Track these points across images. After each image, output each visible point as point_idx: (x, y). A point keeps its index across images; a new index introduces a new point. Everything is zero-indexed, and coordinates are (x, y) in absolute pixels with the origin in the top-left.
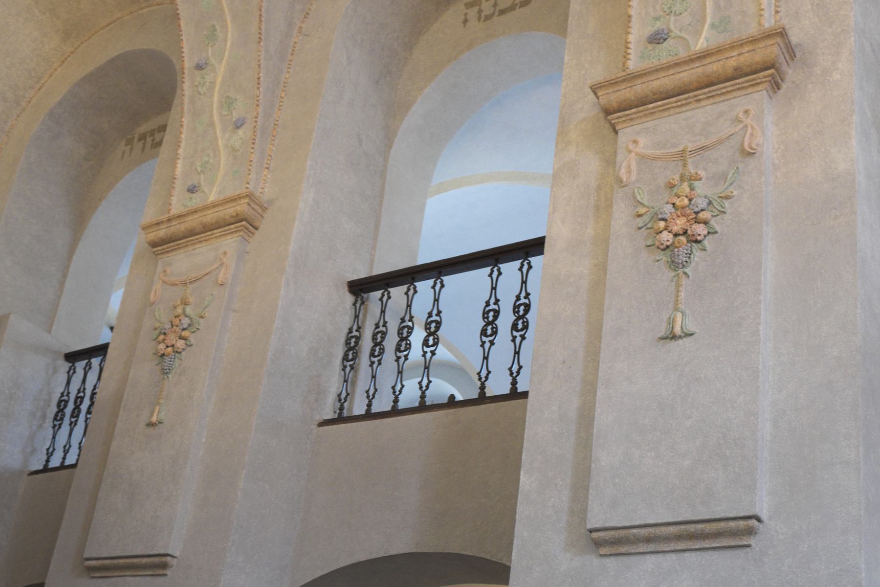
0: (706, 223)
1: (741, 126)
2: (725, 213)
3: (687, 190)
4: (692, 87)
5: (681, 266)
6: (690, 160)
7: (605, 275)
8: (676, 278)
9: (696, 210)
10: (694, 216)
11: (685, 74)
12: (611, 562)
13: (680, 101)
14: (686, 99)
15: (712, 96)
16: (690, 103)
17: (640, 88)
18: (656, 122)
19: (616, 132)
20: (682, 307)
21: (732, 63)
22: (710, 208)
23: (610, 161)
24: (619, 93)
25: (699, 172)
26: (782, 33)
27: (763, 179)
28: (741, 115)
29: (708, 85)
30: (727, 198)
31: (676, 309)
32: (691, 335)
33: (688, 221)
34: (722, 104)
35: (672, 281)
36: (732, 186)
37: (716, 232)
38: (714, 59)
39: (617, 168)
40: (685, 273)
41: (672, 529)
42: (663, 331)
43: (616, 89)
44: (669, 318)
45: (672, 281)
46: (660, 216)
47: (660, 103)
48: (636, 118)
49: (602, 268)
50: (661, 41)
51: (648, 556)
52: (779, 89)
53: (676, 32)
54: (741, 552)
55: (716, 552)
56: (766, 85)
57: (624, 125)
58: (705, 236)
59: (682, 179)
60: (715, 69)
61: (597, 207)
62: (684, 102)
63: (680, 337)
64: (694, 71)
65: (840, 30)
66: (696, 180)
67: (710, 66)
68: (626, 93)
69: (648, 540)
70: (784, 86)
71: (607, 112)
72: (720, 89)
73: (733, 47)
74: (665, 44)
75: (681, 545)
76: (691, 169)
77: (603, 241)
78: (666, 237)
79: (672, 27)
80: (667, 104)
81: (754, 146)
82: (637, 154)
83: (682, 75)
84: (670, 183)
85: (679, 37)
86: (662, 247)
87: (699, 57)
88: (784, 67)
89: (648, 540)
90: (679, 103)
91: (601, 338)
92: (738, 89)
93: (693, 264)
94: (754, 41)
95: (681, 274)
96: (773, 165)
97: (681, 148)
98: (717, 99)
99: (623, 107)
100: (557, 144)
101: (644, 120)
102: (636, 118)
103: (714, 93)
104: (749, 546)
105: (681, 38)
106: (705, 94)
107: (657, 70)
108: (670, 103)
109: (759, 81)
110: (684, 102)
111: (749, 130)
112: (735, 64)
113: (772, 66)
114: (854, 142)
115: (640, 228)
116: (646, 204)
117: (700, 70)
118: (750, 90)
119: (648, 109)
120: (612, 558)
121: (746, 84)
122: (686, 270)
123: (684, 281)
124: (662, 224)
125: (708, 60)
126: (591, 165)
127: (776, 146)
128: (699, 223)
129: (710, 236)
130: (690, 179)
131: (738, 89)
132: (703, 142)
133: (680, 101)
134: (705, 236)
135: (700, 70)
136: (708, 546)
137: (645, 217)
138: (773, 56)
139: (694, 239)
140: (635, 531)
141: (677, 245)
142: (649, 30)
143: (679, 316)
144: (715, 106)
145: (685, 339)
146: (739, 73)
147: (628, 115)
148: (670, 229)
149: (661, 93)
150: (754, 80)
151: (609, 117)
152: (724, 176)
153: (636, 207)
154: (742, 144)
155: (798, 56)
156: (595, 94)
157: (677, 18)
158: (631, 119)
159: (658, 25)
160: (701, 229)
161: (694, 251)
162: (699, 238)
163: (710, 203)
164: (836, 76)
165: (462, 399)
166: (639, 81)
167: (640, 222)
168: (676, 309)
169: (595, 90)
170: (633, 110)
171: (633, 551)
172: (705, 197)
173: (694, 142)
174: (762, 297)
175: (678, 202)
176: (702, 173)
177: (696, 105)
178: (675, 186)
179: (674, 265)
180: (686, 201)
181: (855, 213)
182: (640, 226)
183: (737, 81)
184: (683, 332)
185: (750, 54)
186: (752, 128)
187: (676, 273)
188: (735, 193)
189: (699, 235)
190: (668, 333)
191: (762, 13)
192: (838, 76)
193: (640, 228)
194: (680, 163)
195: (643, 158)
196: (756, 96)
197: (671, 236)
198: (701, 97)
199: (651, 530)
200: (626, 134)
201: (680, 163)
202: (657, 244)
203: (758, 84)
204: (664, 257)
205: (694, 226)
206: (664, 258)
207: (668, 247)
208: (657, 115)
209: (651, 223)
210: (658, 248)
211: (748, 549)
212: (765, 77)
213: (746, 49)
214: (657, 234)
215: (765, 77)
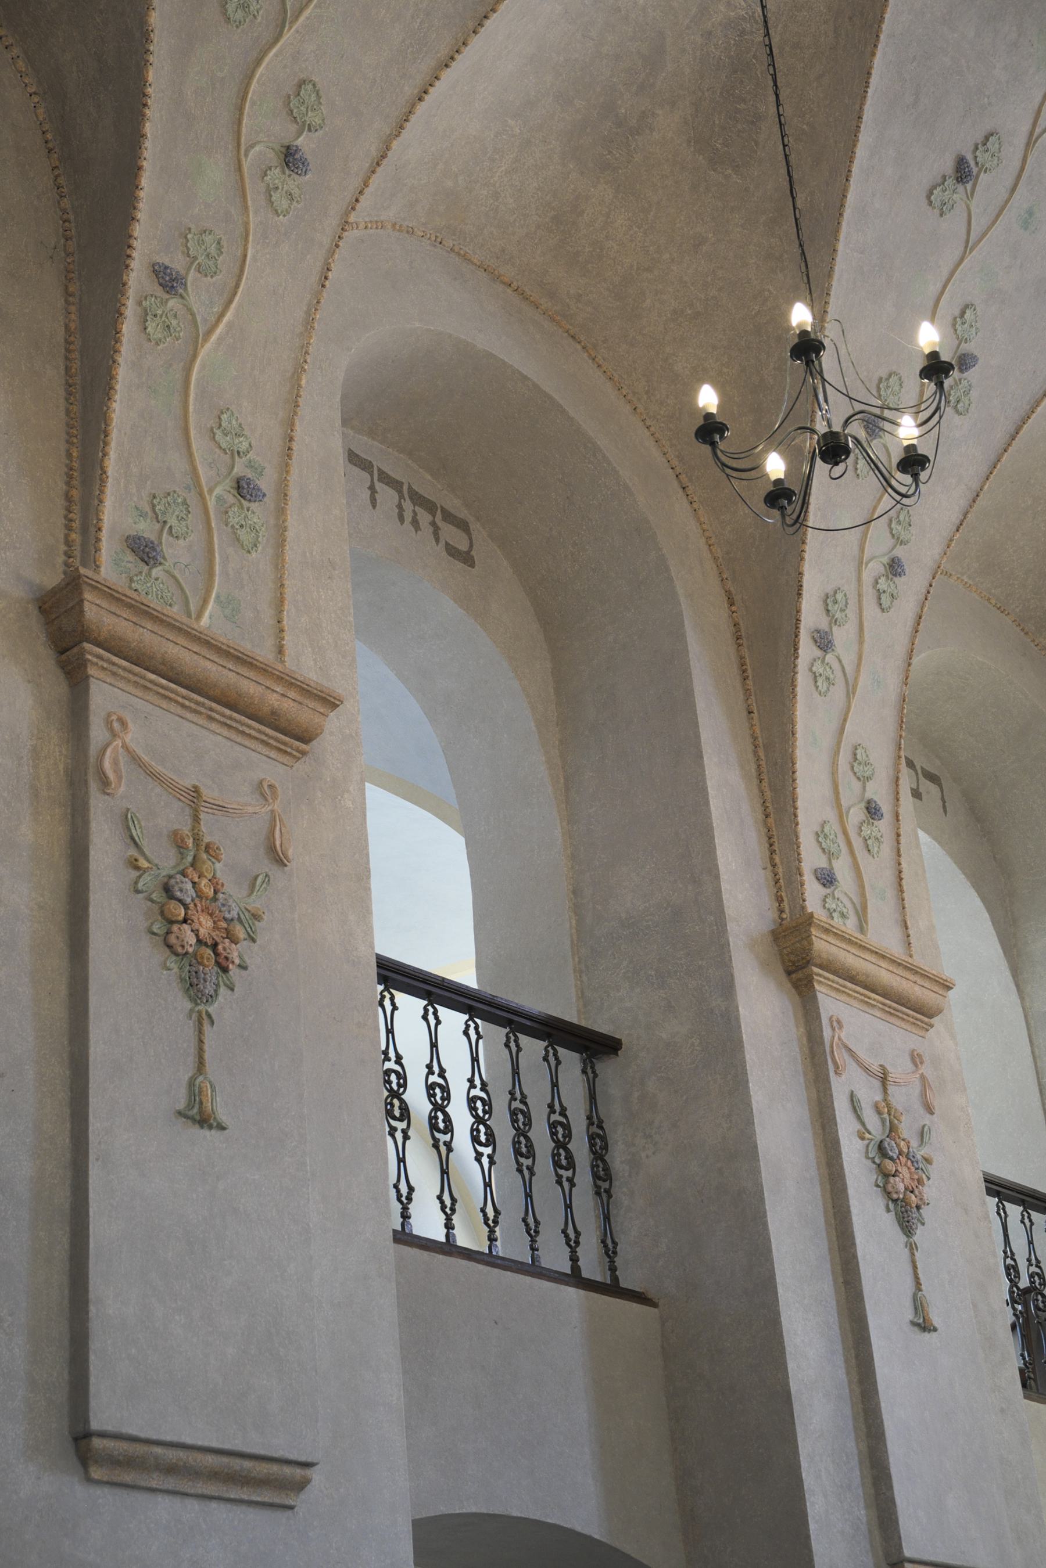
12: (105, 1496)
13: (190, 700)
14: (197, 703)
15: (230, 727)
16: (200, 713)
21: (273, 700)
38: (252, 674)
41: (210, 1459)
47: (164, 682)
48: (122, 678)
51: (160, 1498)
54: (282, 1516)
55: (251, 1510)
69: (171, 1470)
75: (211, 1489)
83: (209, 665)
87: (238, 658)
89: (171, 1470)
90: (187, 703)
92: (263, 742)
101: (130, 688)
102: (122, 678)
103: (234, 724)
104: (291, 1508)
106: (224, 716)
108: (177, 694)
109: (289, 750)
112: (276, 704)
119: (143, 678)
120: (106, 1490)
121: (275, 743)
131: (263, 742)
133: (190, 700)
136: (245, 1497)
140: (158, 1450)
144: (229, 743)
147: (114, 664)
149: (172, 668)
150: (285, 744)
165: (501, 1254)
171: (143, 1484)
198: (217, 716)
199: (182, 1454)
203: (286, 752)
208: (150, 697)
211: (290, 1513)
213: (292, 694)
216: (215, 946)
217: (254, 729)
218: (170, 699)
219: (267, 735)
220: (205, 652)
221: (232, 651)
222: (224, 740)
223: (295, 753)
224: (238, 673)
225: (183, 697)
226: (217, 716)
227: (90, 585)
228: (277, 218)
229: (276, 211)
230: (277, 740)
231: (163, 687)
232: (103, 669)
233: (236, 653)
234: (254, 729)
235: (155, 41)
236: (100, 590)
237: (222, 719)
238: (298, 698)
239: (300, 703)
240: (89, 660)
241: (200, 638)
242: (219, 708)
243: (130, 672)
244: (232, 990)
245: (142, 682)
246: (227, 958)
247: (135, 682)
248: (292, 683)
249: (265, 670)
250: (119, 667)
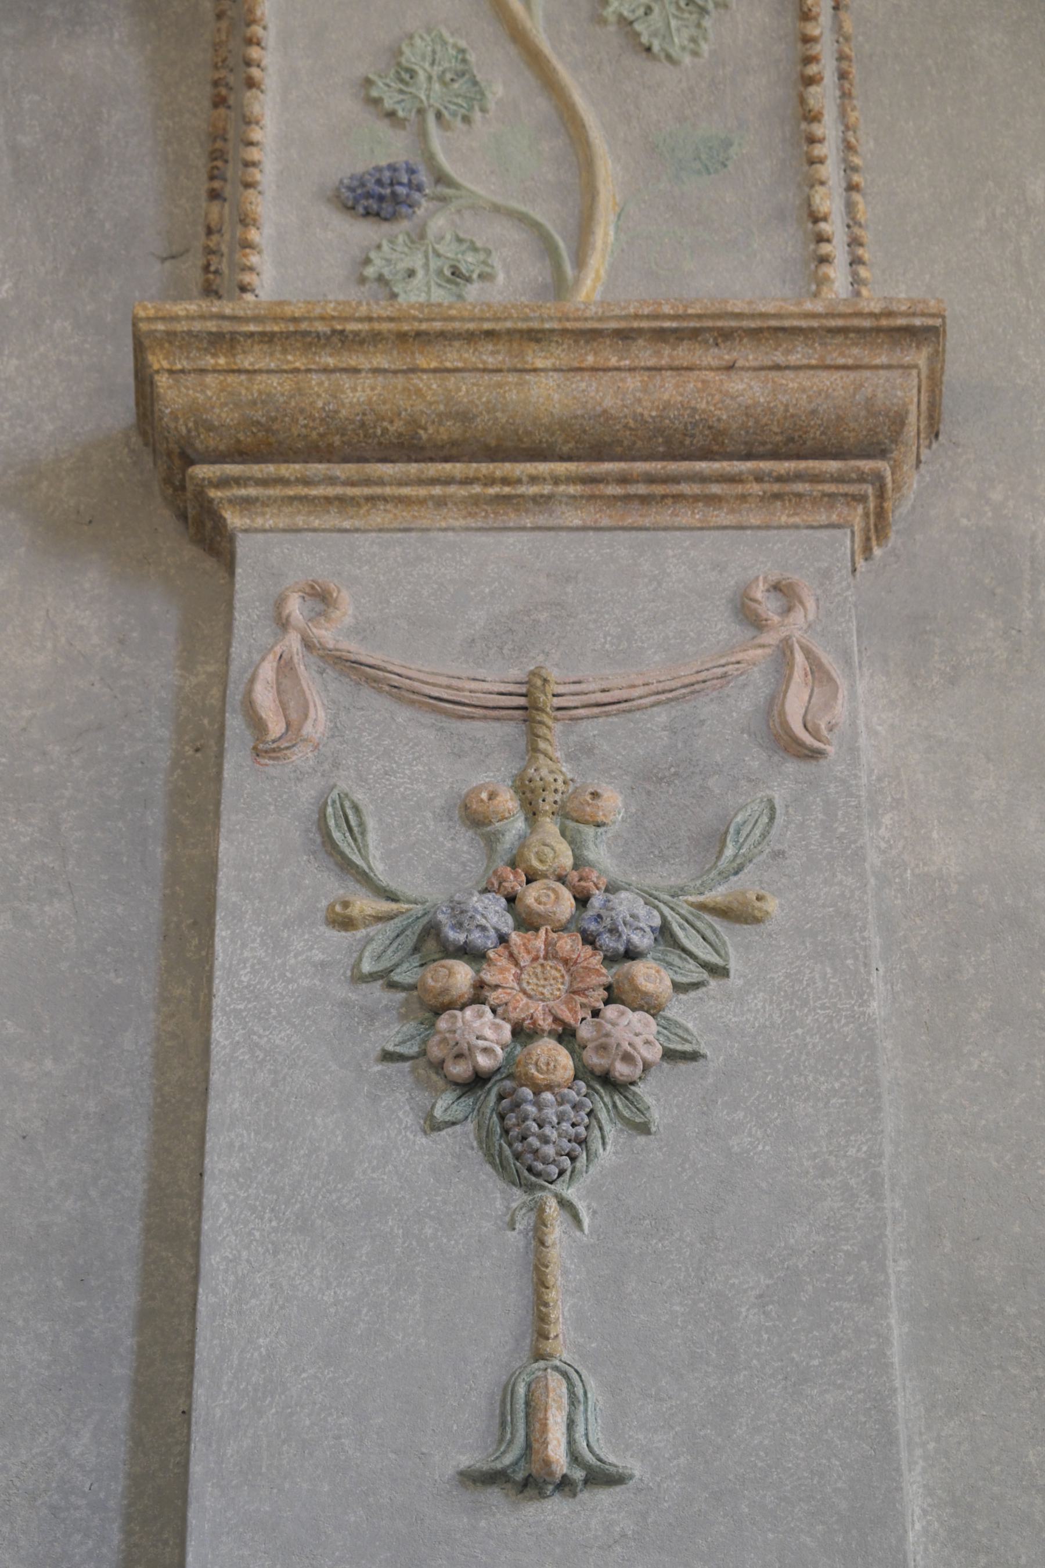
40: (565, 1204)
99: (262, 444)
116: (379, 869)
122: (570, 1193)
202: (436, 1052)
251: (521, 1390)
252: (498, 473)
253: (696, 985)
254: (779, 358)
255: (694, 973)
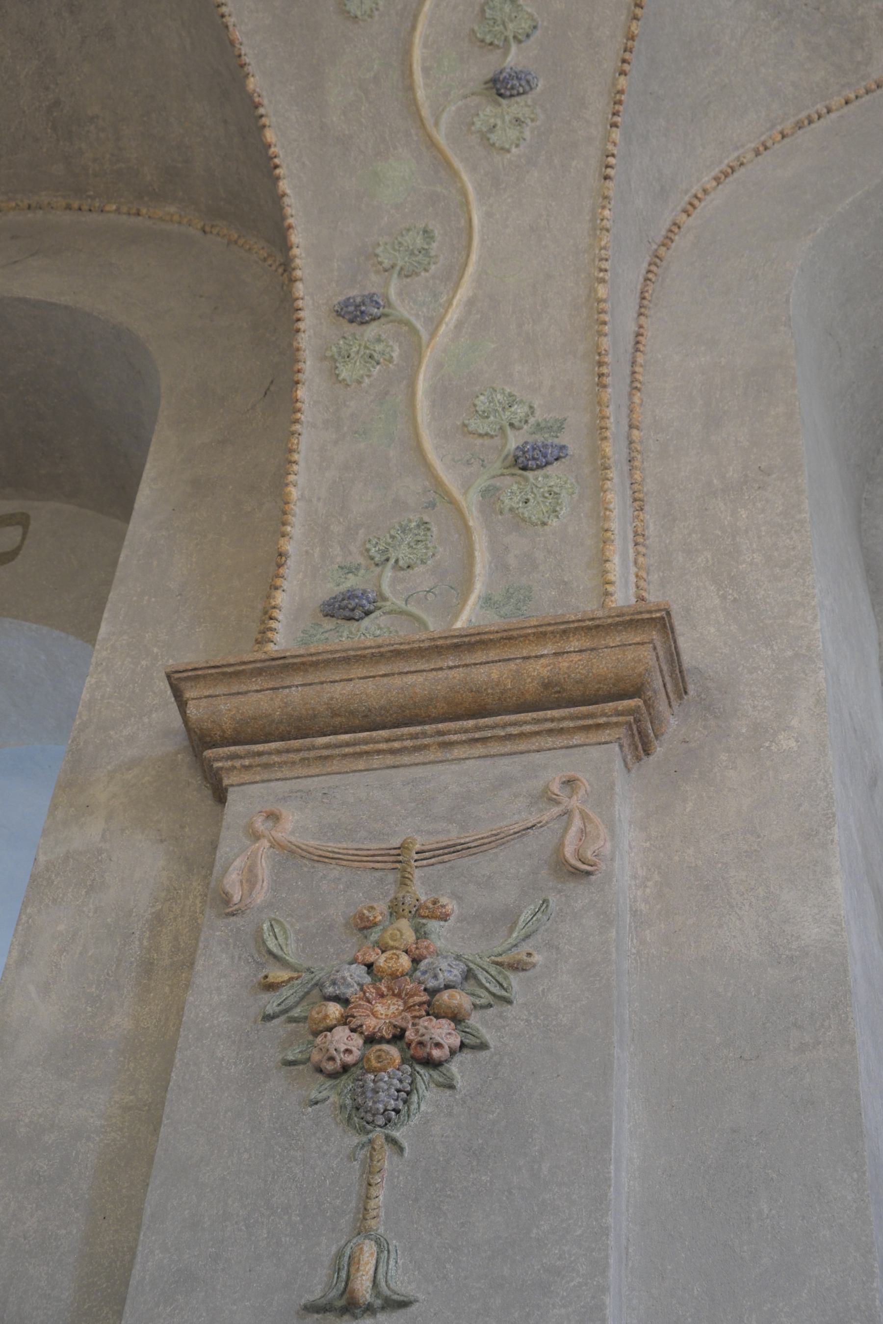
0: (457, 1018)
1: (556, 810)
2: (509, 1002)
3: (410, 936)
4: (434, 713)
5: (381, 1120)
6: (417, 873)
7: (156, 1131)
8: (362, 1154)
9: (432, 983)
10: (425, 998)
11: (420, 678)
16: (426, 747)
17: (298, 695)
18: (335, 779)
19: (220, 796)
20: (379, 1226)
21: (539, 669)
22: (471, 986)
23: (202, 860)
24: (242, 699)
25: (444, 900)
26: (662, 623)
27: (613, 934)
28: (555, 787)
29: (474, 714)
30: (517, 967)
31: (361, 1230)
32: (403, 1304)
33: (408, 1009)
34: (506, 761)
35: (352, 1157)
36: (531, 942)
37: (483, 1046)
38: (493, 655)
39: (217, 868)
40: (392, 1141)
42: (317, 1288)
43: (235, 689)
44: (339, 1255)
45: (352, 1157)
46: (330, 990)
49: (149, 1115)
50: (358, 613)
52: (647, 753)
53: (395, 600)
56: (622, 731)
57: (247, 777)
58: (453, 1052)
59: (395, 911)
60: (495, 676)
61: (148, 968)
62: (409, 743)
63: (369, 1309)
64: (441, 674)
65: (789, 653)
66: (433, 916)
67: (482, 669)
68: (259, 701)
70: (659, 750)
71: (200, 740)
72: (504, 726)
73: (544, 634)
74: (366, 622)
76: (420, 891)
77: (157, 1054)
78: (344, 1041)
79: (386, 589)
80: (365, 742)
81: (589, 854)
82: (275, 844)
83: (410, 679)
84: (362, 917)
85: (402, 612)
86: (330, 1067)
87: (456, 646)
88: (662, 705)
90: (397, 745)
91: (123, 1301)
92: (550, 732)
93: (415, 1120)
94: (593, 628)
95: (381, 1141)
96: (634, 913)
97: (396, 842)
98: (495, 748)
99: (249, 734)
100: (54, 807)
102: (281, 764)
103: (489, 733)
105: (409, 614)
106: (466, 731)
107: (347, 660)
110: (409, 743)
111: (577, 823)
112: (545, 672)
113: (637, 691)
114: (838, 883)
115: (268, 1018)
116: (291, 959)
117: (457, 675)
118: (577, 739)
119: (314, 748)
121: (571, 724)
122: (396, 1134)
123: (387, 1160)
124: (334, 1010)
125: (480, 656)
126: (140, 867)
127: (641, 873)
128: (438, 1017)
129: (467, 1056)
130: (417, 914)
131: (550, 732)
132: (454, 835)
134: (453, 1052)
135: (457, 675)
137: (285, 992)
138: (641, 669)
139: (421, 1053)
141: (374, 1063)
142: (329, 589)
143: (369, 1252)
144: (488, 762)
145: (381, 1317)
146: (553, 696)
147: (260, 754)
148: (355, 1023)
149: (352, 713)
150: (591, 716)
151: (209, 753)
152: (509, 918)
153: (261, 965)
154: (560, 846)
155: (692, 692)
156: (178, 694)
157: (401, 574)
158: (266, 766)
159: (351, 582)
160: (443, 1033)
161: (421, 1086)
162: (436, 1053)
163: (469, 975)
164: (787, 742)
166: (298, 680)
167: (271, 1002)
168: (361, 1230)
169: (177, 683)
170: (273, 745)
172: (458, 958)
173: (429, 833)
174: (610, 1220)
175: (381, 961)
176: (450, 905)
177: (440, 755)
178: (376, 924)
179: (361, 1116)
180: (405, 962)
181: (853, 1043)
182: (270, 1010)
183: (549, 714)
184: (378, 1295)
185: (584, 655)
186: (584, 817)
187: (364, 1139)
188: (537, 958)
189: (438, 1045)
190: (334, 1293)
191: (610, 588)
192: (792, 743)
193: (268, 1018)
194: (391, 877)
195: (290, 854)
196: (594, 753)
197: (357, 1041)
198: (454, 738)
200: (245, 800)
201: (391, 877)
202: (316, 1057)
203: (598, 726)
204: (333, 1095)
205: (424, 1022)
206: (334, 1098)
207: (346, 1068)
208: (335, 766)
209: (297, 1007)
210: (320, 1070)
212: (619, 714)
213: (575, 644)
214: (316, 1034)
215: (619, 714)
216: (398, 1037)
217: (526, 723)
218: (367, 753)
219: (552, 720)
220: (401, 666)
221: (440, 642)
222: (479, 762)
223: (614, 719)
224: (466, 665)
225: (388, 740)
226: (454, 738)
227: (188, 678)
228: (508, 156)
229: (502, 149)
230: (572, 718)
231: (348, 744)
232: (247, 768)
233: (449, 642)
234: (526, 723)
235: (265, 102)
236: (204, 677)
237: (464, 737)
238: (588, 644)
239: (592, 649)
240: (221, 768)
241: (382, 655)
242: (452, 725)
243: (288, 751)
244: (452, 1087)
245: (312, 754)
246: (421, 1044)
247: (302, 760)
248: (564, 632)
249: (510, 638)
250: (270, 753)
251: (348, 1252)
252: (549, 716)
253: (490, 1006)
254: (440, 664)
255: (486, 999)
